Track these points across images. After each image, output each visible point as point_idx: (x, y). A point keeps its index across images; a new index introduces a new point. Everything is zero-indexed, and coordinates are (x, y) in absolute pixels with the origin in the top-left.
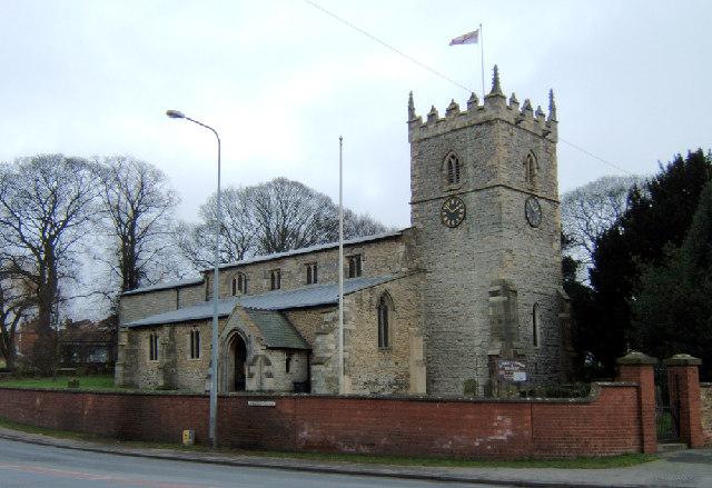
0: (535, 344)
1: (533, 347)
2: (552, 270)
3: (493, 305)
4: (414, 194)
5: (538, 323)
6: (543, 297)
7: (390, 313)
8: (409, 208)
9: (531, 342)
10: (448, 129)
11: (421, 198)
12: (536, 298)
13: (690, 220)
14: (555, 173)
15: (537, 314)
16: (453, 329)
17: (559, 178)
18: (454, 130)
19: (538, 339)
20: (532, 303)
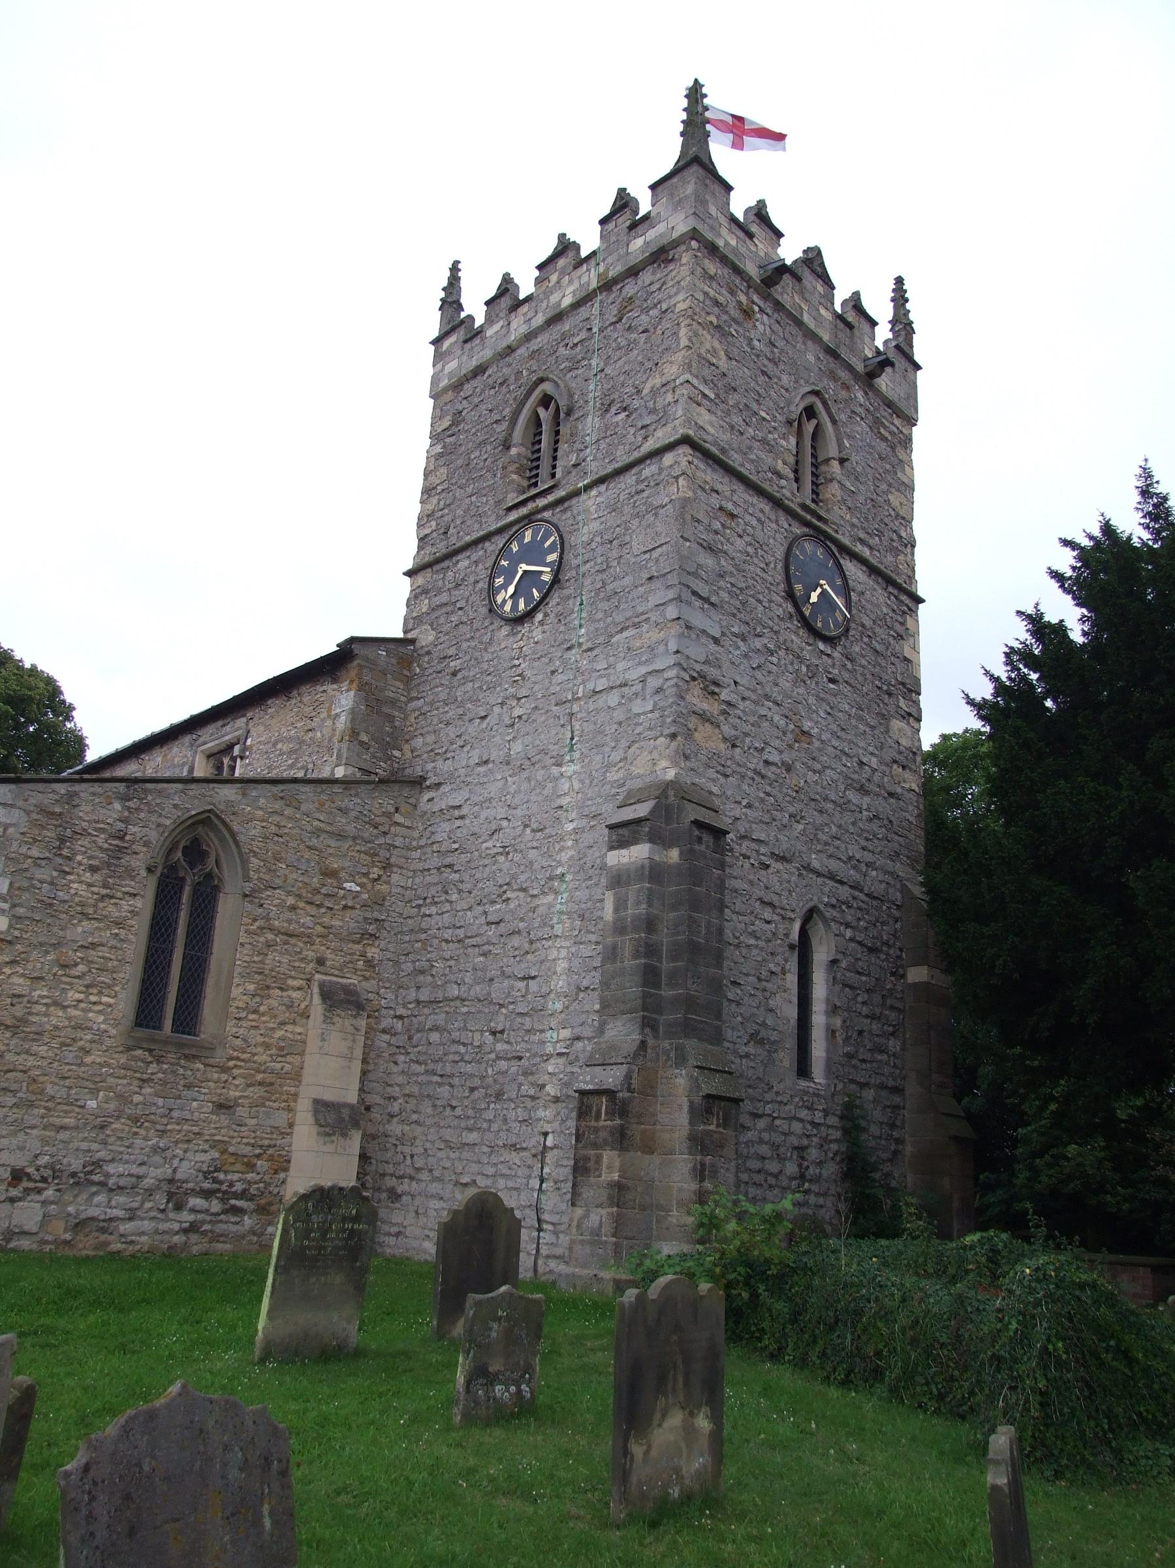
0: (803, 1069)
1: (791, 1082)
2: (884, 807)
3: (618, 880)
4: (422, 540)
5: (820, 990)
6: (844, 892)
7: (227, 908)
8: (405, 586)
9: (786, 1059)
10: (539, 320)
11: (441, 548)
12: (821, 893)
13: (257, 1330)
14: (915, 649)
15: (821, 955)
16: (479, 991)
17: (920, 528)
18: (558, 317)
19: (818, 1050)
20: (802, 908)
